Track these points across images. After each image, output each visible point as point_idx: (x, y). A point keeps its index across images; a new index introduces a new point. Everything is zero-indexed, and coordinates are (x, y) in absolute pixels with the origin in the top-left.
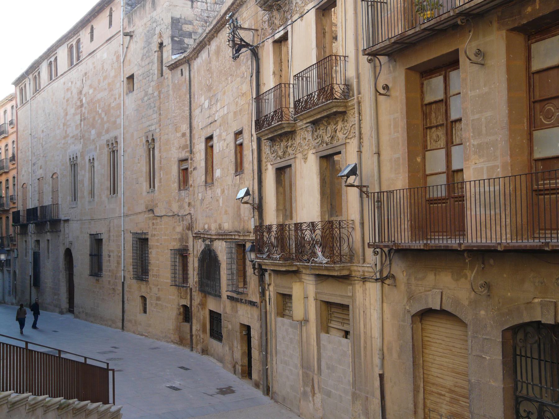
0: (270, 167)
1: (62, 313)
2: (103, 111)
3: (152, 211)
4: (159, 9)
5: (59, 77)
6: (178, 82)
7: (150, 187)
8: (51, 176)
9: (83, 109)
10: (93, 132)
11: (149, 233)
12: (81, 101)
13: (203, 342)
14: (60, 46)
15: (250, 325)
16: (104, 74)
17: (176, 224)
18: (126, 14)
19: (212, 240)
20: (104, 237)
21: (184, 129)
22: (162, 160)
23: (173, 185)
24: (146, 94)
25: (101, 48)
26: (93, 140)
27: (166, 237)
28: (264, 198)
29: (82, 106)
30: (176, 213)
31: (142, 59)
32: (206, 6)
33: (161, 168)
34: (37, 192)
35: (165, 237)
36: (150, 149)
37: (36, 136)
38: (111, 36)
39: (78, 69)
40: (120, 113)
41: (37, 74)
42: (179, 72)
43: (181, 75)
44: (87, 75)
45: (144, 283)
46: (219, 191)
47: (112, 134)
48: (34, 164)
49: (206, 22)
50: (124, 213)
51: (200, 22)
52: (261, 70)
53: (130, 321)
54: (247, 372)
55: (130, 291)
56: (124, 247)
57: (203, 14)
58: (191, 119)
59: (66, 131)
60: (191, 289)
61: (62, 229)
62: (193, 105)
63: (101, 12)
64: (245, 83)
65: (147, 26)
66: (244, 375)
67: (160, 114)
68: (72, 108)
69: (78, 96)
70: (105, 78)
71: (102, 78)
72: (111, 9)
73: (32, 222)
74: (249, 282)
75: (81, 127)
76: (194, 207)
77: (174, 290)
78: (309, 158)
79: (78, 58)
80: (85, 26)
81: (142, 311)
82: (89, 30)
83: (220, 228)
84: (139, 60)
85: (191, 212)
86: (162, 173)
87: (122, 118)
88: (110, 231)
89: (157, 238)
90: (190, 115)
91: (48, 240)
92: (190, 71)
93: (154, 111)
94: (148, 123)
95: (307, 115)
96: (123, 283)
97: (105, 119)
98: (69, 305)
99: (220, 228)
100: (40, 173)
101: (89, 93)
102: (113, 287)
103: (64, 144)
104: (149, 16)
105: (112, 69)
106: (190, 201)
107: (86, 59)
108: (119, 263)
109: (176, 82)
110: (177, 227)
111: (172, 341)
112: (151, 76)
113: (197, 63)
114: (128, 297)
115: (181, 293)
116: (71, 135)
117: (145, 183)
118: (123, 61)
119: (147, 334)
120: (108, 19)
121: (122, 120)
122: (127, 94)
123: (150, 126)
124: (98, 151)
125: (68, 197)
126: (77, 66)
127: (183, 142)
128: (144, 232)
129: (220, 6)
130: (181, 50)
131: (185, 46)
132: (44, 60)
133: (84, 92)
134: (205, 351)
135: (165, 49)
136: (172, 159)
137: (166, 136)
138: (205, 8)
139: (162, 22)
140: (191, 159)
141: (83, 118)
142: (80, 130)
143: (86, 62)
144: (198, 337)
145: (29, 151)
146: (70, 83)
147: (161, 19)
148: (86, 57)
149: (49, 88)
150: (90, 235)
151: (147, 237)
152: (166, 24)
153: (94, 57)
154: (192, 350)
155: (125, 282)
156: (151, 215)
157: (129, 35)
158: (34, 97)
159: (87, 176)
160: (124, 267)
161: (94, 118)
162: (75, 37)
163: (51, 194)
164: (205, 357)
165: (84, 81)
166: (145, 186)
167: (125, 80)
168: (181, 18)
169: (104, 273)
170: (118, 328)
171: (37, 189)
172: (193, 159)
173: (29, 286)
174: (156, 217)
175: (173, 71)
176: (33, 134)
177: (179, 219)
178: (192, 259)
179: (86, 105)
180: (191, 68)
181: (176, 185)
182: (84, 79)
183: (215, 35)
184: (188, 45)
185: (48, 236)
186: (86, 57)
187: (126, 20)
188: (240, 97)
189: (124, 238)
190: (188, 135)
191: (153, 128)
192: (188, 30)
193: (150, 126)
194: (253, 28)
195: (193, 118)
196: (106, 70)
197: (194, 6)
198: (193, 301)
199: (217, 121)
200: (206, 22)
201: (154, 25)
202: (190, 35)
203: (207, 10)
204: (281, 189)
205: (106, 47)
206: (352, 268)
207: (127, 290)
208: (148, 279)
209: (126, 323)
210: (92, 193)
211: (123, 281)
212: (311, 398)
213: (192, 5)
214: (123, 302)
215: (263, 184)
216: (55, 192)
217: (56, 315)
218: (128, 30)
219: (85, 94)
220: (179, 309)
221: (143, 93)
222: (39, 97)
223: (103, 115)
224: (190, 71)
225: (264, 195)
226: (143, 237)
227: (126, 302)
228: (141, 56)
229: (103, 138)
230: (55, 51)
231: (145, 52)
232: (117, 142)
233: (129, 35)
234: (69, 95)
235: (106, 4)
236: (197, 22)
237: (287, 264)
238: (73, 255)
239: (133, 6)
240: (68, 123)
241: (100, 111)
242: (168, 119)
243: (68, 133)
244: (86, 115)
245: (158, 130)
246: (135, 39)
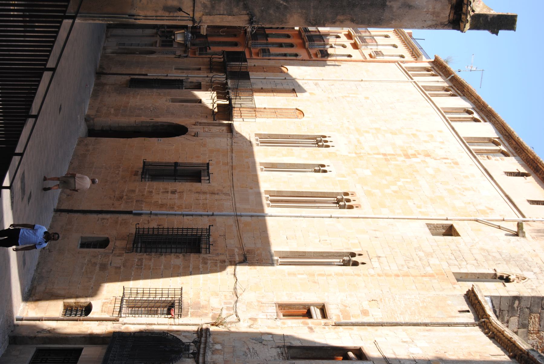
102: (125, 197)
160: (156, 215)
227: (100, 216)
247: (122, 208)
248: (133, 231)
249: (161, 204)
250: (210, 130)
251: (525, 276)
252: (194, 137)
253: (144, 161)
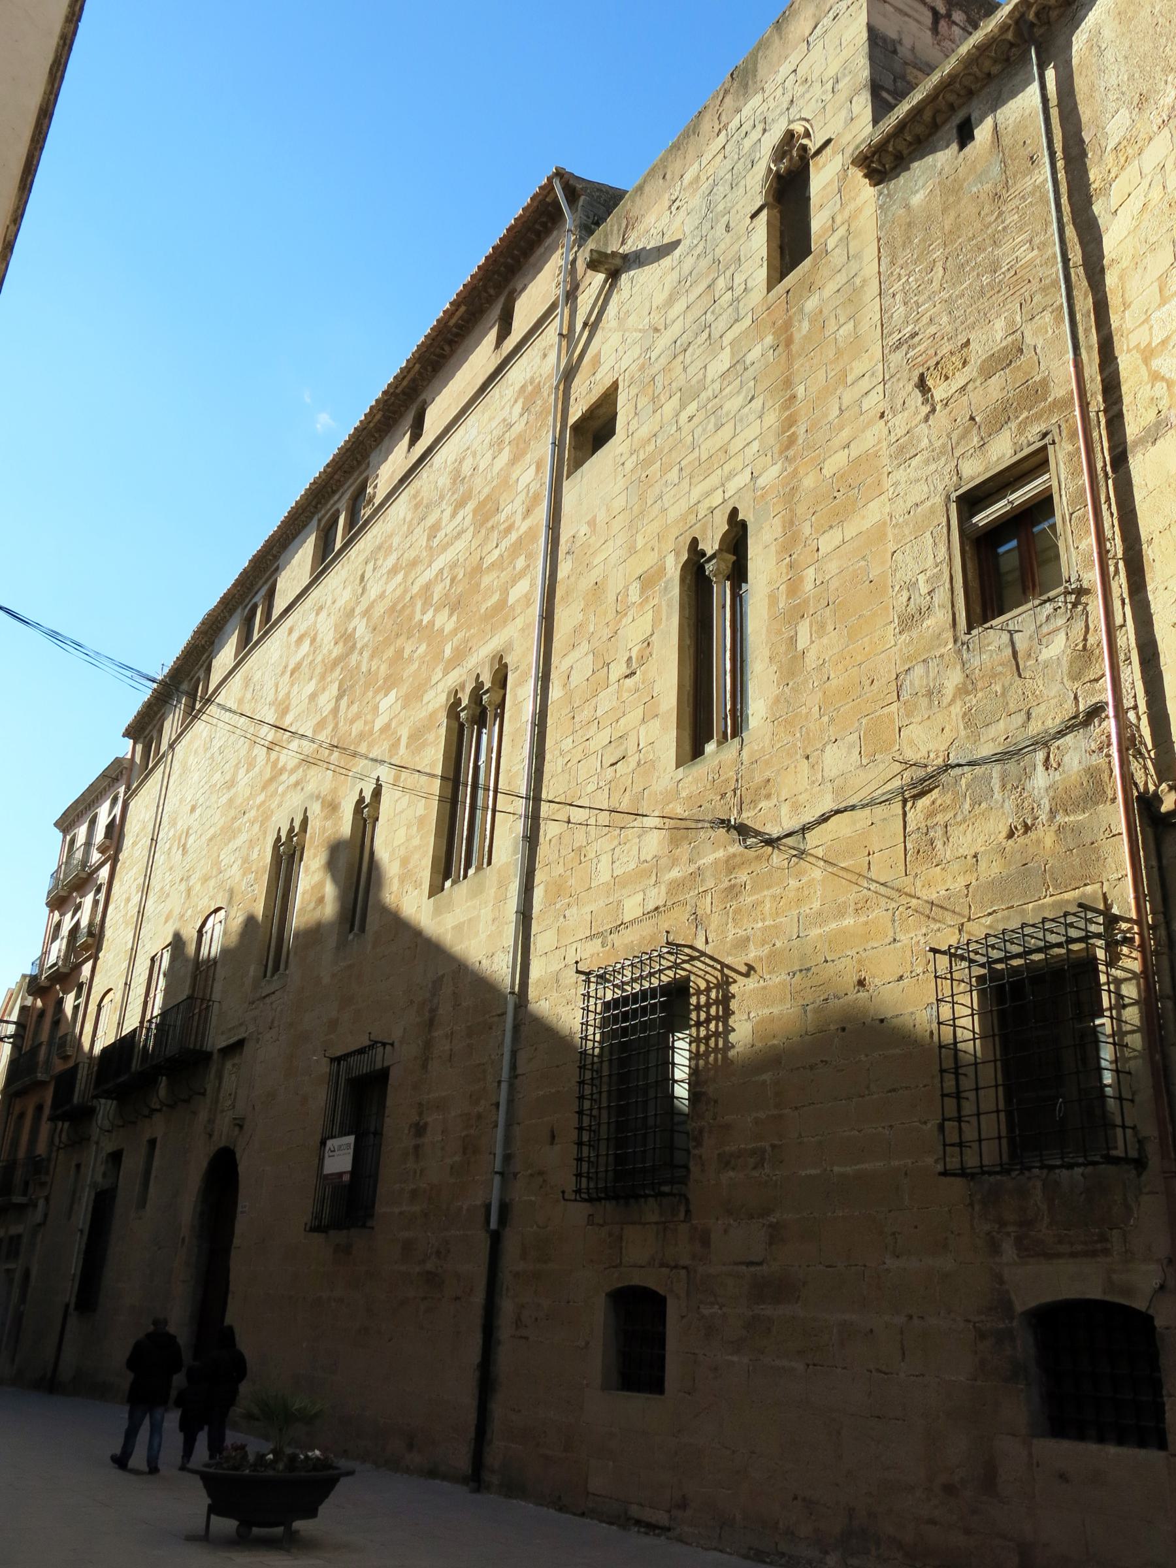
81: (1083, 901)
102: (429, 1266)
132: (231, 612)
160: (507, 1158)
168: (900, 42)
211: (493, 1225)
227: (505, 1332)
247: (477, 1269)
248: (579, 1211)
249: (464, 1153)
250: (230, 1095)
251: (572, 533)
252: (245, 1127)
253: (308, 1229)
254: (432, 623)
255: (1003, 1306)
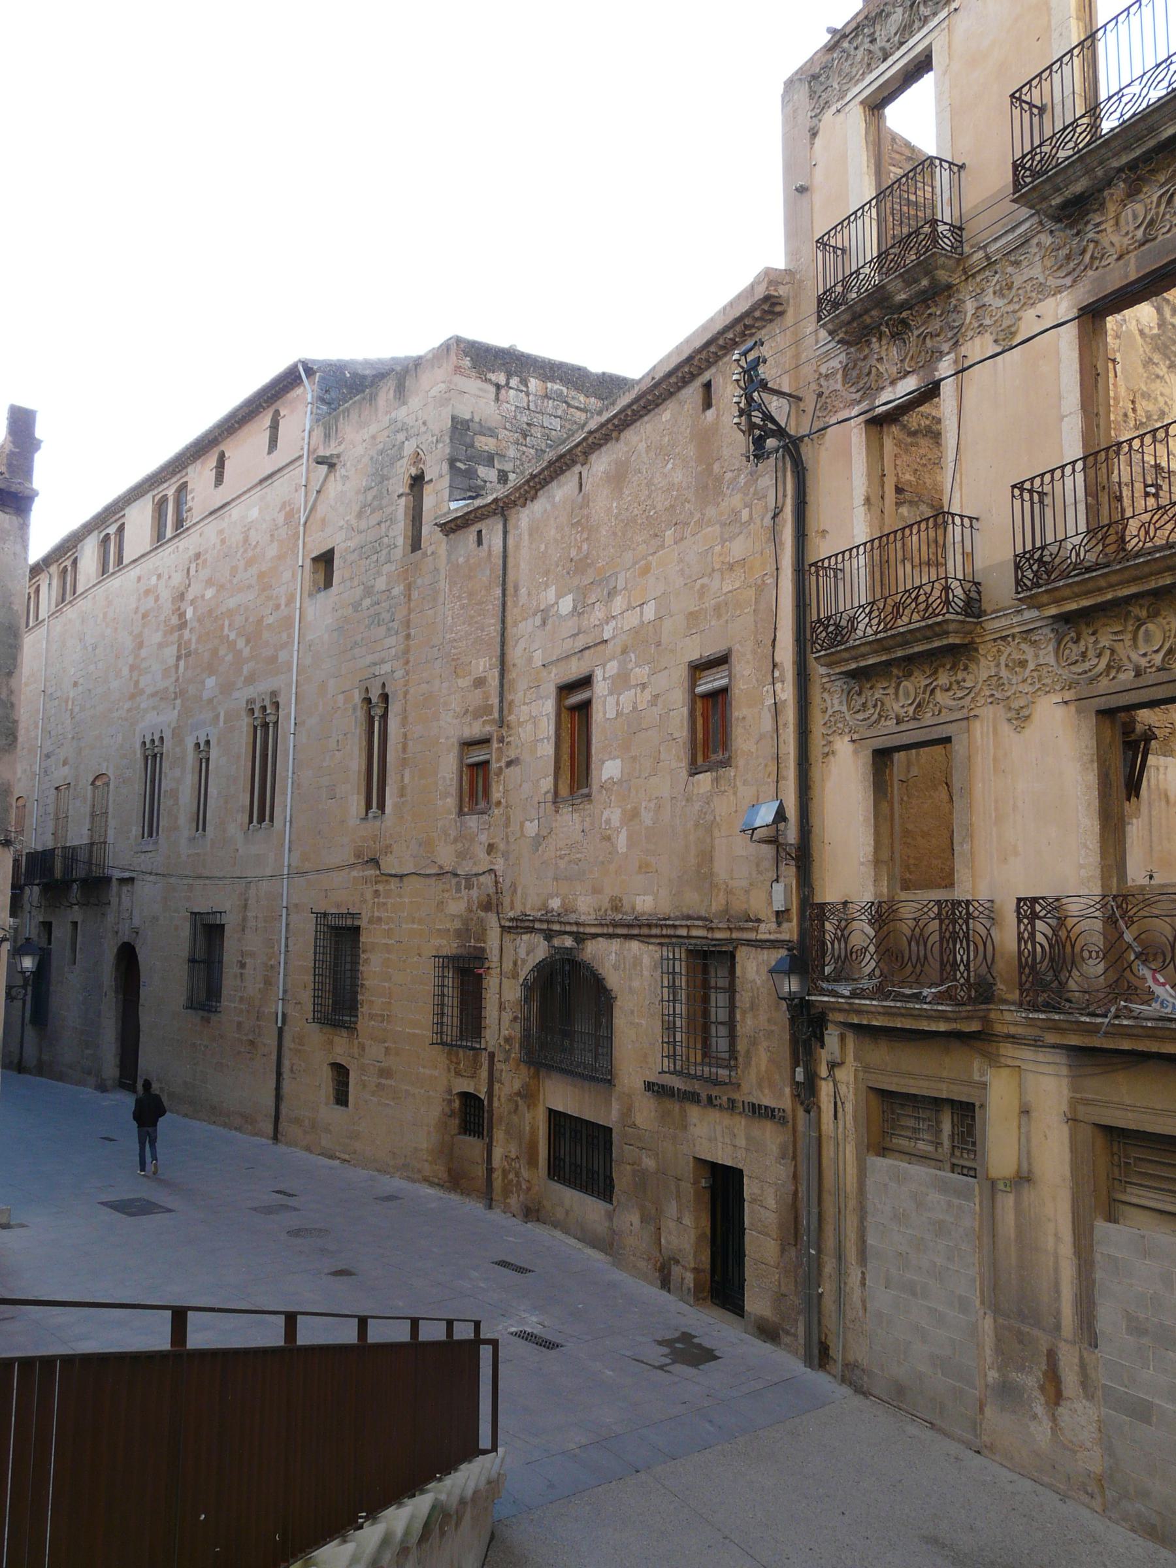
0: (843, 746)
1: (102, 1088)
2: (239, 635)
3: (374, 862)
4: (415, 402)
5: (127, 566)
6: (467, 561)
7: (197, 830)
8: (91, 780)
9: (186, 633)
10: (211, 682)
11: (364, 914)
12: (182, 615)
13: (529, 1189)
14: (135, 500)
15: (740, 1166)
16: (250, 553)
17: (446, 895)
18: (318, 420)
19: (580, 938)
20: (230, 921)
21: (481, 669)
22: (410, 743)
23: (440, 803)
24: (368, 591)
25: (243, 498)
26: (210, 701)
27: (415, 926)
28: (816, 830)
29: (183, 625)
30: (447, 869)
31: (360, 515)
32: (526, 399)
33: (404, 763)
34: (52, 816)
35: (410, 926)
36: (373, 717)
37: (59, 694)
38: (276, 469)
39: (177, 547)
40: (291, 636)
41: (68, 563)
42: (473, 537)
43: (476, 544)
44: (202, 558)
45: (344, 1033)
46: (614, 815)
47: (263, 687)
48: (48, 756)
49: (525, 436)
50: (289, 866)
51: (512, 434)
52: (810, 498)
53: (297, 1121)
54: (708, 1287)
55: (300, 1051)
56: (287, 946)
57: (518, 418)
58: (503, 644)
59: (137, 683)
60: (492, 1056)
61: (114, 900)
62: (512, 613)
63: (250, 420)
64: (742, 537)
65: (378, 440)
66: (701, 1295)
67: (408, 636)
68: (157, 631)
69: (173, 603)
70: (250, 563)
71: (242, 564)
72: (277, 413)
73: (37, 881)
74: (748, 1052)
75: (177, 672)
76: (506, 855)
77: (439, 1056)
78: (1036, 717)
79: (179, 523)
80: (204, 454)
82: (212, 461)
83: (616, 908)
84: (351, 518)
85: (496, 867)
86: (407, 773)
87: (296, 647)
88: (245, 906)
89: (386, 927)
90: (503, 635)
91: (75, 924)
92: (505, 533)
93: (389, 629)
94: (369, 659)
95: (1083, 588)
96: (281, 1031)
97: (246, 652)
98: (121, 1071)
99: (616, 908)
100: (61, 774)
101: (203, 596)
102: (251, 1037)
103: (129, 710)
104: (386, 420)
105: (272, 541)
106: (491, 841)
107: (202, 524)
108: (268, 982)
109: (461, 560)
110: (450, 901)
111: (426, 1180)
112: (384, 552)
113: (524, 518)
114: (292, 1065)
115: (458, 1063)
116: (149, 691)
117: (355, 797)
118: (306, 523)
119: (347, 1157)
120: (267, 433)
121: (296, 653)
122: (310, 595)
123: (375, 664)
124: (221, 723)
125: (134, 829)
126: (177, 540)
127: (475, 698)
128: (350, 911)
129: (556, 403)
130: (470, 490)
131: (480, 482)
132: (90, 532)
133: (190, 596)
134: (532, 1213)
135: (428, 490)
136: (442, 740)
137: (424, 686)
138: (525, 405)
139: (423, 429)
140: (501, 740)
141: (183, 652)
142: (173, 679)
143: (199, 532)
144: (511, 1176)
145: (36, 727)
146: (155, 578)
147: (420, 422)
148: (202, 519)
149: (100, 591)
150: (192, 913)
151: (356, 923)
152: (437, 432)
153: (223, 519)
154: (490, 1207)
155: (286, 1028)
156: (371, 872)
157: (329, 463)
158: (57, 611)
159: (190, 780)
160: (285, 992)
161: (215, 652)
162: (174, 479)
163: (88, 820)
164: (534, 1229)
165: (192, 572)
166: (356, 803)
167: (308, 563)
168: (472, 420)
169: (225, 1003)
170: (262, 1136)
171: (51, 809)
172: (506, 740)
173: (19, 1022)
174: (385, 878)
175: (452, 536)
176: (49, 691)
177: (458, 884)
178: (497, 981)
179: (195, 624)
180: (510, 527)
181: (451, 802)
182: (193, 566)
183: (614, 434)
184: (485, 482)
185: (76, 914)
186: (202, 519)
187: (318, 433)
188: (717, 575)
189: (287, 925)
190: (494, 682)
191: (386, 668)
192: (486, 448)
193: (375, 664)
194: (786, 389)
195: (510, 642)
196: (254, 543)
197: (501, 397)
198: (496, 1086)
199: (610, 645)
200: (525, 436)
201: (401, 437)
202: (489, 460)
203: (529, 409)
204: (885, 806)
205: (257, 494)
206: (993, 1015)
207: (292, 1046)
208: (356, 1023)
209: (283, 1125)
210: (200, 820)
211: (279, 1025)
212: (1039, 1409)
213: (497, 394)
214: (279, 1074)
215: (816, 792)
216: (98, 815)
217: (88, 1093)
218: (322, 452)
219: (192, 601)
220: (450, 1102)
221: (359, 591)
222: (70, 613)
223: (241, 643)
224: (505, 533)
225: (815, 821)
226: (349, 922)
227: (286, 1074)
228: (356, 508)
229: (236, 694)
230: (120, 512)
231: (370, 498)
232: (277, 705)
233: (329, 463)
234: (150, 602)
235: (266, 402)
236: (507, 433)
237: (964, 1014)
238: (140, 958)
239: (333, 406)
240: (144, 665)
241: (232, 636)
242: (433, 647)
243: (142, 685)
244: (193, 646)
245: (399, 674)
246: (340, 471)
249: (265, 984)
254: (235, 642)
255: (450, 1091)
